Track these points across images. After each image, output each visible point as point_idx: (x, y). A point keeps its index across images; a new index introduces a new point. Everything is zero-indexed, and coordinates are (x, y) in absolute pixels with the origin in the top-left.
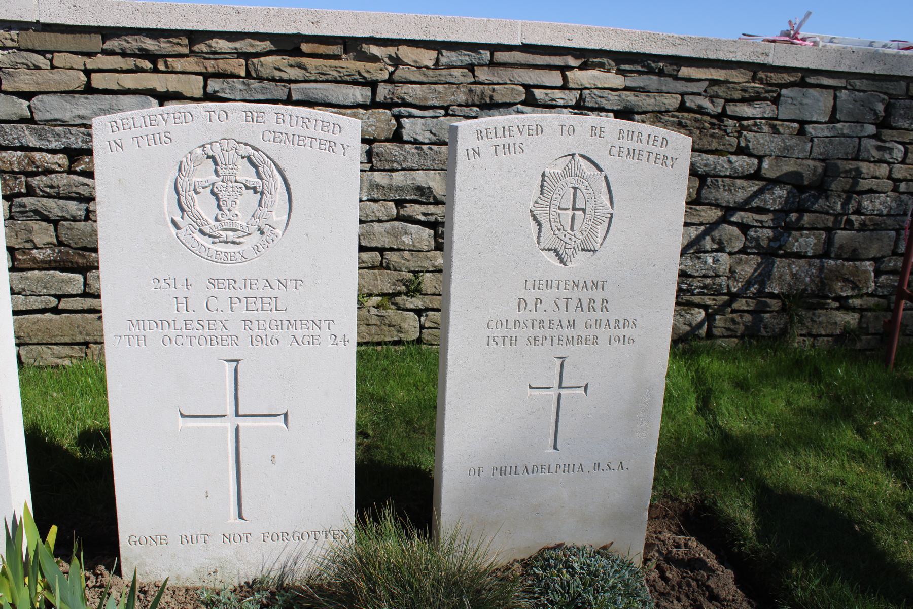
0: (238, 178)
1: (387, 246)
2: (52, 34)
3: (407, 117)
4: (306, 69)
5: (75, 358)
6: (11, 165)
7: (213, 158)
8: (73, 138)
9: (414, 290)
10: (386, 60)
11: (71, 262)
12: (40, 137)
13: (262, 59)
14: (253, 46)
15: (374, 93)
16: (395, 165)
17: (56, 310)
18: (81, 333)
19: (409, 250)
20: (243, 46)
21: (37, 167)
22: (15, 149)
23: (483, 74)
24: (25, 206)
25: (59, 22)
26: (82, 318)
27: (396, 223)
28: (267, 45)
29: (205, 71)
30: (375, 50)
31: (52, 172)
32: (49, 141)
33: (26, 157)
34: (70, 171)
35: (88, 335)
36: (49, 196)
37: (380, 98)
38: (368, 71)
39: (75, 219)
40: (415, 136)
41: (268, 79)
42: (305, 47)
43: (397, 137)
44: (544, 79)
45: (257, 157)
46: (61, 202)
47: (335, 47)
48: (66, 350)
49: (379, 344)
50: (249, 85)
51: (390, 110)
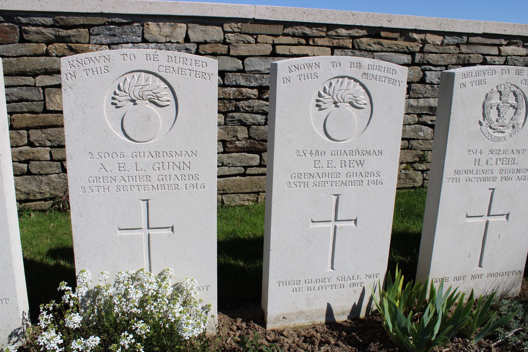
0: (509, 102)
1: (412, 137)
2: (259, 25)
3: (428, 71)
4: (382, 45)
5: (251, 201)
6: (229, 95)
7: (500, 92)
8: (264, 81)
9: (422, 159)
10: (419, 41)
11: (256, 148)
12: (247, 80)
13: (361, 39)
14: (357, 32)
15: (413, 58)
16: (420, 96)
17: (244, 175)
18: (256, 187)
19: (422, 140)
20: (352, 32)
21: (243, 96)
22: (232, 86)
23: (464, 49)
24: (234, 117)
25: (264, 19)
26: (258, 178)
27: (417, 125)
28: (364, 32)
29: (332, 45)
30: (415, 36)
31: (251, 98)
32: (251, 82)
33: (237, 91)
34: (259, 98)
35: (260, 188)
36: (247, 112)
37: (417, 61)
38: (412, 47)
39: (259, 124)
40: (432, 81)
41: (363, 50)
42: (383, 34)
43: (422, 81)
44: (491, 51)
45: (518, 91)
46: (253, 115)
47: (396, 34)
48: (247, 197)
49: (404, 188)
50: (354, 53)
51: (420, 67)
